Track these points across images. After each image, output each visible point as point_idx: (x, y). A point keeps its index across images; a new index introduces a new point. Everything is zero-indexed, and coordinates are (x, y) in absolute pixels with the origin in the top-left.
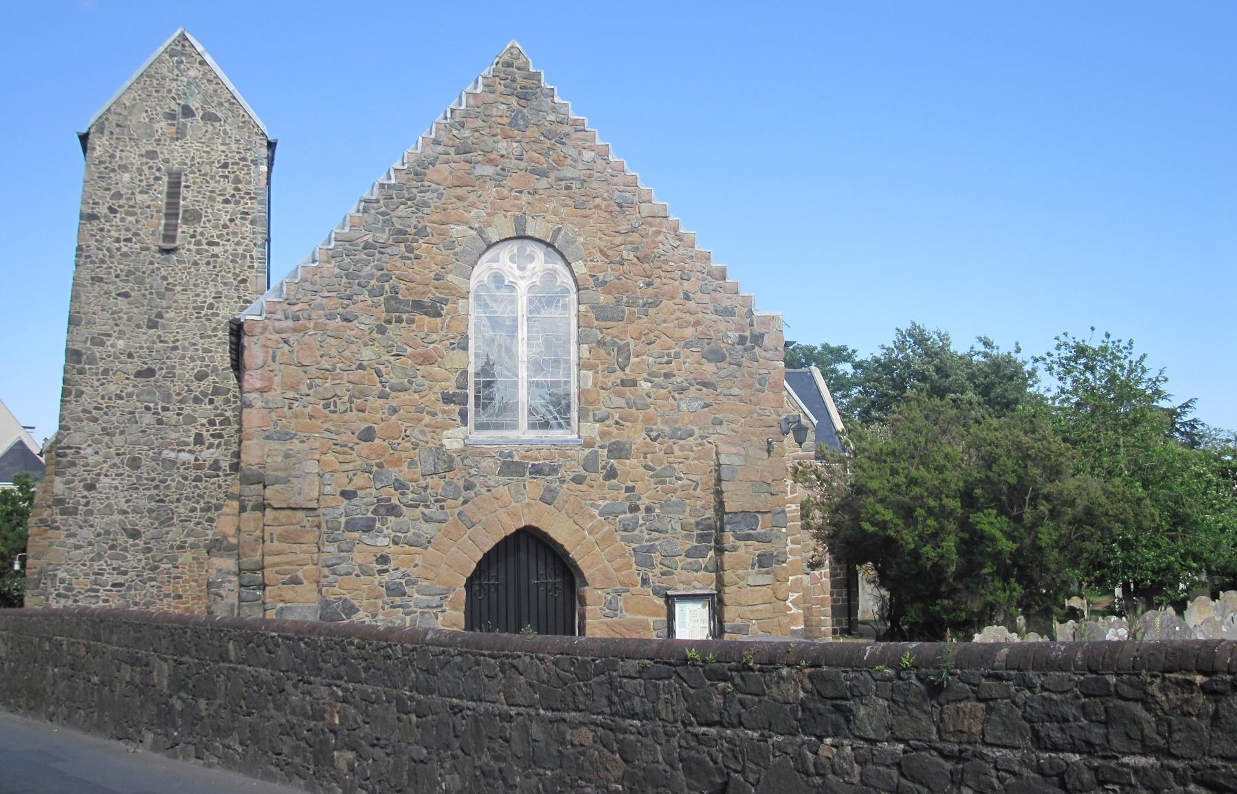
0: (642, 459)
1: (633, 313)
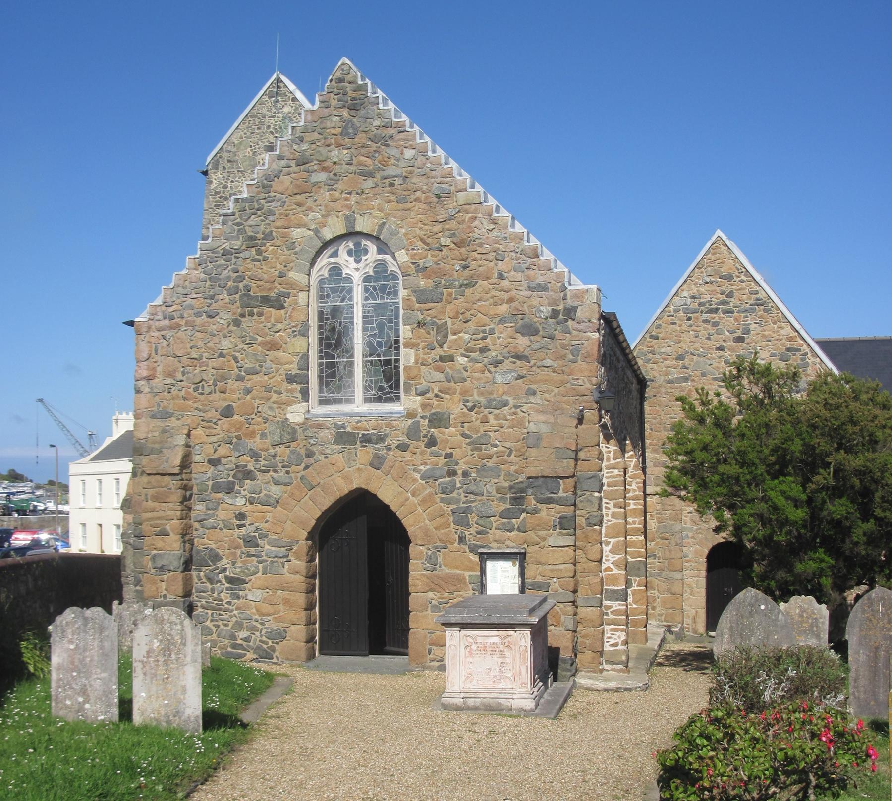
0: (459, 428)
1: (450, 295)
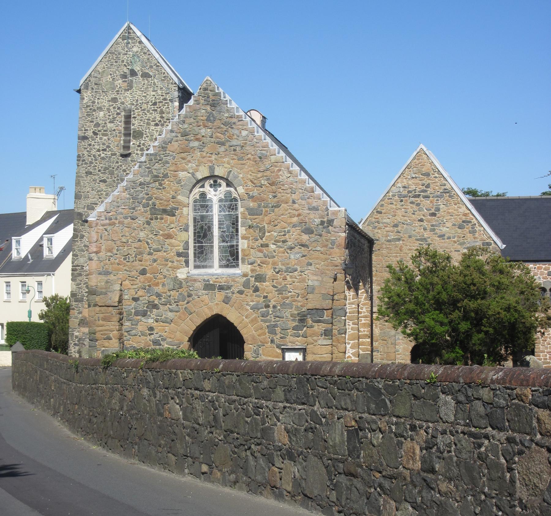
0: (271, 282)
1: (267, 211)
